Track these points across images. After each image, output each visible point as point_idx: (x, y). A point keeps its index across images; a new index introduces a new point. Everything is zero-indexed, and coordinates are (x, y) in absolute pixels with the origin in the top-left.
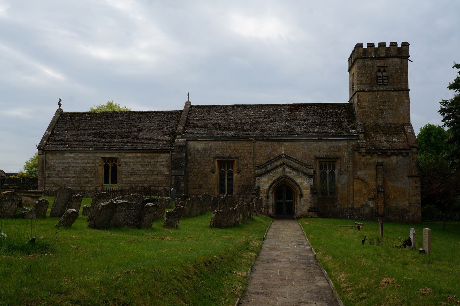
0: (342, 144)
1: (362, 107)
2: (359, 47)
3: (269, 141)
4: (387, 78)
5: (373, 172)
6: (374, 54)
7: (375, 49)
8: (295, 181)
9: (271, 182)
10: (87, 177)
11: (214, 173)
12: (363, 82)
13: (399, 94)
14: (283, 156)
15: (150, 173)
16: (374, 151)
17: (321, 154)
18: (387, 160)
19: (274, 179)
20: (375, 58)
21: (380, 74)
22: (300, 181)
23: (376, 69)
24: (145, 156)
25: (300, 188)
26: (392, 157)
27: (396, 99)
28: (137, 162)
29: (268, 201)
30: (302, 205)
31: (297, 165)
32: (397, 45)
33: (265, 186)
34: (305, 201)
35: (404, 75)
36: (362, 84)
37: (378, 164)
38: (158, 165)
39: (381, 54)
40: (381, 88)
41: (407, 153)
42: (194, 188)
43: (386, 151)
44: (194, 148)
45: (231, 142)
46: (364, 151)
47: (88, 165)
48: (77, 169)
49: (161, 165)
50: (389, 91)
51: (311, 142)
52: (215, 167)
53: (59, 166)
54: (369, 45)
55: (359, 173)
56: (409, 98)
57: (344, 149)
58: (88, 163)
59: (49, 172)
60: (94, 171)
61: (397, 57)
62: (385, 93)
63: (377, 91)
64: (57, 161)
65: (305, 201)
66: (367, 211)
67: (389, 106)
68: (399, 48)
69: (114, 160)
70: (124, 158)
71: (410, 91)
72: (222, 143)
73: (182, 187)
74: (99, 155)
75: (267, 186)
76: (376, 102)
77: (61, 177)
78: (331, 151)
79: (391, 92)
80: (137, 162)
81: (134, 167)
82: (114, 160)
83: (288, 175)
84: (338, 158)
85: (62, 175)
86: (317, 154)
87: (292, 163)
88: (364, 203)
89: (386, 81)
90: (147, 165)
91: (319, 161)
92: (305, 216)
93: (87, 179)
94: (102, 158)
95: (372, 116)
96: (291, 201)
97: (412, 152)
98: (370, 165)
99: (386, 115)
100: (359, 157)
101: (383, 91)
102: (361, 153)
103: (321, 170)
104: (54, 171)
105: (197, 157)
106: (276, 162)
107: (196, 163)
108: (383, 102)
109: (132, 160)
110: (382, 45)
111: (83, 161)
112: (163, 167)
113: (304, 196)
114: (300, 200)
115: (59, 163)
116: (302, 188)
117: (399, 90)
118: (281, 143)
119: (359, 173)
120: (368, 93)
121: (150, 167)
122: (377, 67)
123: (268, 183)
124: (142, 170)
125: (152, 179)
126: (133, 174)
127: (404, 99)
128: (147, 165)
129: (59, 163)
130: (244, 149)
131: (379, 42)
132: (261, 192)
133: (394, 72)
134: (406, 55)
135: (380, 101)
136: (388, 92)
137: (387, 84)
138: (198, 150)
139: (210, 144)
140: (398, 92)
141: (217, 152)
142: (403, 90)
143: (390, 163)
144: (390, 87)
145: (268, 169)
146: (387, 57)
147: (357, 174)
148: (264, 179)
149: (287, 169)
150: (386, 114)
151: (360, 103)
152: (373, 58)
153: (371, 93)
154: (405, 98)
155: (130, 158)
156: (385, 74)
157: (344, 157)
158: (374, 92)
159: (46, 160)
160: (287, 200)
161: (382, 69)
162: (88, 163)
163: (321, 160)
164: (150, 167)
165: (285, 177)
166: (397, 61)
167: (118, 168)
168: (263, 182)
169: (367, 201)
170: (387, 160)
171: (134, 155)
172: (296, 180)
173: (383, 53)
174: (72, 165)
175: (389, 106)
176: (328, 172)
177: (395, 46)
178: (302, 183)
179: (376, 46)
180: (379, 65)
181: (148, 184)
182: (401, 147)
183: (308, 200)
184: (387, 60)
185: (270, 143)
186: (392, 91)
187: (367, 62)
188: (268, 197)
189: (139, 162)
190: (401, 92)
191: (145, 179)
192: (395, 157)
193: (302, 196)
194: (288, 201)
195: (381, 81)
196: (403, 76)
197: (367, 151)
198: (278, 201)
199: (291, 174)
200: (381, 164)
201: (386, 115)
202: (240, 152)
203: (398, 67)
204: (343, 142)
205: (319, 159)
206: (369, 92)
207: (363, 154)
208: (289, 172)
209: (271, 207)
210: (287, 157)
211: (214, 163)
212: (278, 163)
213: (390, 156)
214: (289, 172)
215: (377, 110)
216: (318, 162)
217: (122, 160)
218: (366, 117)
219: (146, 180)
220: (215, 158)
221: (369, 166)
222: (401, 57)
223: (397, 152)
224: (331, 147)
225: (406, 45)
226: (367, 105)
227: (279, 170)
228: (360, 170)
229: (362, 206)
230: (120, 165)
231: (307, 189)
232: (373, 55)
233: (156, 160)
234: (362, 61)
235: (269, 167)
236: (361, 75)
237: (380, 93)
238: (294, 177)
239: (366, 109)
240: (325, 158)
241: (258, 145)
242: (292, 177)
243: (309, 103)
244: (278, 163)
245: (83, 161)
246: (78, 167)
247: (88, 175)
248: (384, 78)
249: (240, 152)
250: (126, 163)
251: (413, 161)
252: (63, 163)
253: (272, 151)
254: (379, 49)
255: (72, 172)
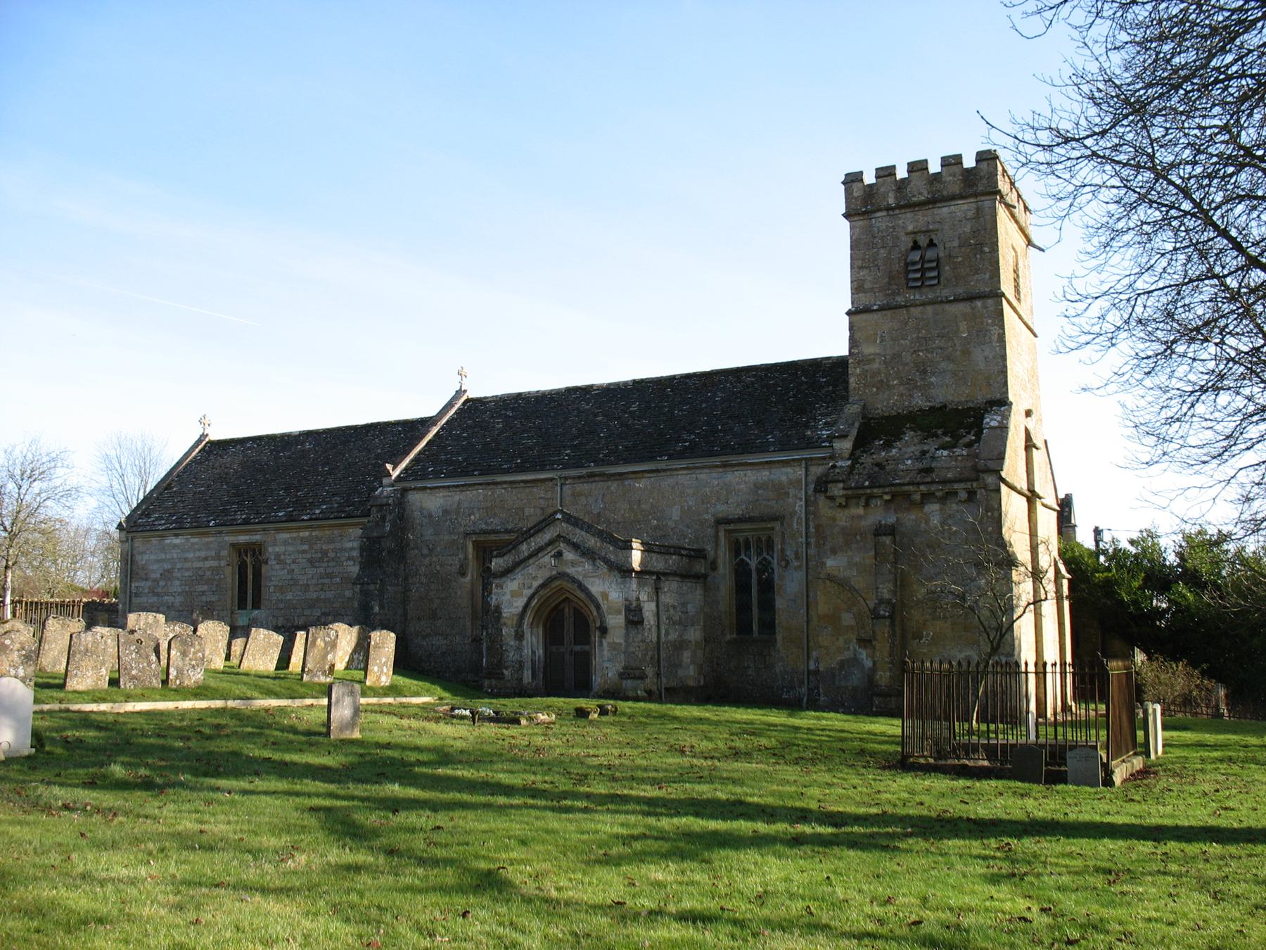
0: (783, 475)
1: (862, 361)
2: (853, 181)
3: (597, 479)
4: (934, 264)
5: (868, 557)
6: (896, 198)
7: (868, 189)
8: (587, 589)
9: (528, 592)
10: (203, 592)
11: (463, 574)
12: (867, 285)
13: (973, 308)
14: (559, 516)
15: (326, 581)
16: (869, 491)
17: (732, 509)
18: (913, 517)
19: (536, 584)
20: (899, 207)
21: (916, 256)
22: (601, 589)
23: (906, 242)
24: (317, 537)
25: (598, 607)
26: (926, 507)
27: (963, 326)
28: (299, 552)
29: (519, 649)
30: (606, 659)
31: (592, 542)
32: (961, 163)
33: (515, 605)
34: (614, 649)
35: (986, 249)
36: (865, 291)
37: (879, 531)
38: (343, 559)
39: (914, 196)
40: (916, 296)
41: (971, 494)
42: (419, 618)
43: (906, 488)
44: (421, 510)
45: (505, 489)
46: (842, 493)
47: (208, 564)
48: (187, 574)
49: (349, 559)
50: (942, 302)
51: (703, 476)
52: (466, 558)
53: (155, 567)
54: (882, 173)
55: (830, 563)
56: (1003, 320)
57: (792, 492)
58: (206, 559)
59: (137, 584)
60: (217, 577)
61: (962, 197)
62: (930, 309)
63: (906, 306)
64: (153, 557)
65: (613, 646)
66: (856, 679)
67: (941, 348)
68: (969, 171)
69: (255, 550)
70: (275, 544)
71: (849, 306)
72: (486, 492)
73: (376, 614)
74: (226, 538)
75: (520, 603)
76: (903, 342)
77: (158, 594)
78: (757, 500)
79: (947, 307)
80: (299, 552)
81: (293, 566)
82: (255, 550)
83: (571, 571)
84: (775, 518)
85: (159, 590)
86: (722, 509)
87: (579, 535)
88: (847, 655)
89: (934, 274)
90: (321, 560)
91: (725, 530)
92: (613, 693)
93: (204, 599)
94: (233, 545)
95: (894, 386)
96: (587, 648)
97: (984, 488)
98: (861, 535)
99: (933, 379)
100: (829, 513)
101: (923, 304)
102: (832, 498)
103: (736, 557)
104: (147, 580)
105: (429, 533)
106: (540, 535)
107: (425, 551)
108: (925, 338)
109: (290, 548)
110: (918, 167)
111: (198, 554)
112: (352, 563)
113: (611, 632)
114: (601, 644)
115: (158, 561)
116: (604, 607)
117: (971, 298)
118: (627, 483)
119: (830, 563)
120: (880, 313)
121: (326, 565)
122: (907, 234)
123: (521, 595)
124: (311, 571)
125: (330, 595)
126: (292, 583)
127: (988, 324)
128: (321, 560)
129: (158, 561)
130: (535, 507)
131: (910, 161)
132: (505, 624)
133: (956, 244)
134: (988, 189)
135: (915, 336)
136: (937, 306)
137: (935, 282)
138: (431, 516)
139: (457, 497)
140: (969, 303)
141: (472, 517)
142: (982, 296)
143: (923, 525)
144: (945, 292)
145: (522, 556)
146: (933, 202)
147: (824, 564)
148: (512, 585)
149: (569, 555)
150: (933, 374)
151: (857, 346)
152: (893, 209)
153: (889, 313)
154: (990, 321)
155: (285, 543)
156: (930, 254)
157: (793, 514)
158: (897, 311)
159: (132, 556)
160: (575, 644)
161: (923, 241)
162: (206, 559)
163: (732, 527)
164: (326, 565)
165: (562, 575)
166: (963, 208)
167: (264, 569)
168: (508, 593)
169: (855, 650)
170: (913, 517)
171: (294, 535)
172: (590, 587)
173: (920, 191)
174: (179, 566)
175: (941, 348)
176: (753, 563)
177: (954, 167)
178: (605, 596)
179: (902, 173)
180: (910, 228)
181: (321, 609)
182: (949, 475)
183: (620, 644)
184: (936, 211)
185: (600, 485)
186: (951, 301)
187: (877, 224)
188: (519, 636)
189: (304, 552)
190: (979, 303)
191: (315, 595)
192: (936, 507)
193: (604, 630)
194: (578, 648)
195: (918, 275)
196: (982, 252)
197: (850, 492)
198: (554, 649)
199: (580, 569)
200: (891, 531)
201: (933, 379)
202: (527, 514)
203: (967, 229)
204: (789, 470)
205: (726, 523)
206: (884, 312)
207: (839, 500)
208: (573, 564)
209: (528, 665)
210: (568, 519)
211: (464, 548)
212: (547, 536)
213: (922, 504)
214: (573, 564)
215: (907, 364)
216: (722, 534)
217: (270, 549)
218: (875, 390)
219: (318, 600)
220: (467, 534)
221: (858, 538)
222: (975, 195)
223: (939, 490)
224: (757, 486)
225: (987, 158)
226: (877, 351)
227: (547, 559)
228: (834, 552)
229: (842, 664)
230: (266, 563)
231: (618, 612)
232: (891, 201)
233: (338, 545)
234: (861, 223)
235: (525, 549)
236: (860, 263)
237: (915, 311)
238: (585, 576)
239: (876, 366)
240: (740, 520)
241: (570, 492)
242: (581, 578)
243: (796, 359)
244: (547, 536)
245: (198, 554)
246: (188, 569)
247: (205, 588)
248: (926, 266)
249: (527, 514)
250: (278, 555)
251: (988, 517)
252: (163, 561)
253: (605, 508)
254: (910, 182)
255: (177, 583)
